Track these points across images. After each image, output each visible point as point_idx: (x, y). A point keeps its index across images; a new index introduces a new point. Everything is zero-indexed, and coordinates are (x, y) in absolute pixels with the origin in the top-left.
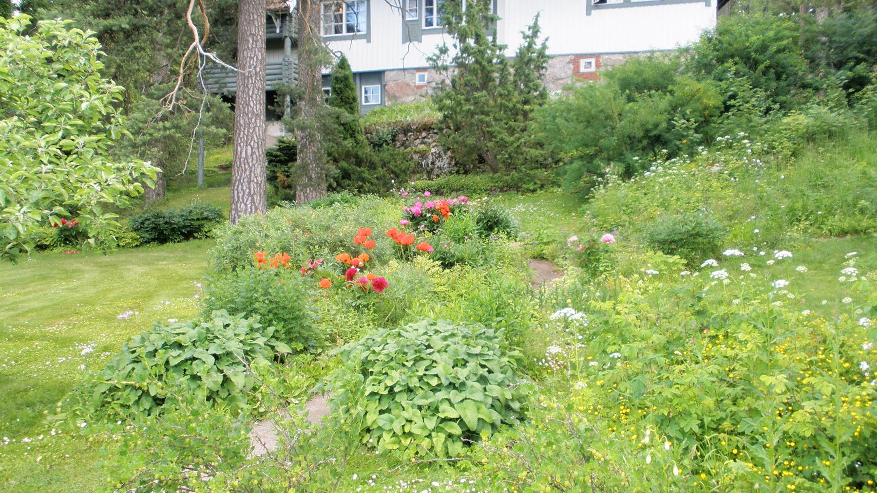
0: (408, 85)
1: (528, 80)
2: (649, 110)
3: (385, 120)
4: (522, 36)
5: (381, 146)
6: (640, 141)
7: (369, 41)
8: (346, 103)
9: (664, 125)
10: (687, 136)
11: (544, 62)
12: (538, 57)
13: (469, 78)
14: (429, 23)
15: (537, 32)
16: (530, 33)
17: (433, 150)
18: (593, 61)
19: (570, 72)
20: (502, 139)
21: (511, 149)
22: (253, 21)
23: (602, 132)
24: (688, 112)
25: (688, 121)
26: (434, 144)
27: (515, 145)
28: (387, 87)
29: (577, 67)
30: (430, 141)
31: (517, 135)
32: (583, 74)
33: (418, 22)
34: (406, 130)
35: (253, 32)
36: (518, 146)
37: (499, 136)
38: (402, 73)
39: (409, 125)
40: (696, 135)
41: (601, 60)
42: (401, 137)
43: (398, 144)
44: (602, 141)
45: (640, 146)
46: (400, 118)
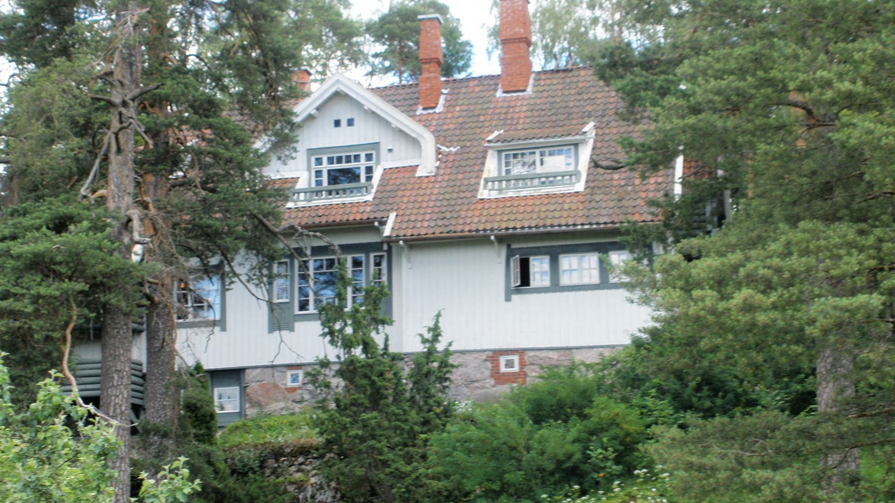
0: (276, 387)
1: (428, 396)
2: (558, 439)
3: (250, 441)
4: (419, 339)
5: (245, 474)
6: (552, 474)
7: (224, 329)
8: (202, 422)
9: (578, 456)
10: (605, 468)
11: (448, 372)
12: (440, 367)
13: (356, 396)
14: (303, 306)
15: (439, 335)
16: (428, 336)
17: (313, 480)
18: (516, 358)
19: (487, 373)
20: (397, 469)
21: (408, 481)
22: (119, 356)
23: (506, 467)
24: (605, 440)
25: (606, 449)
26: (314, 472)
27: (414, 476)
28: (248, 390)
29: (496, 366)
30: (309, 468)
31: (415, 464)
32: (504, 374)
33: (289, 304)
34: (278, 453)
35: (119, 368)
36: (417, 478)
37: (394, 466)
38: (270, 371)
39: (281, 448)
40: (614, 467)
41: (526, 357)
42: (271, 463)
43: (268, 472)
44: (507, 476)
45: (552, 480)
46: (269, 437)
